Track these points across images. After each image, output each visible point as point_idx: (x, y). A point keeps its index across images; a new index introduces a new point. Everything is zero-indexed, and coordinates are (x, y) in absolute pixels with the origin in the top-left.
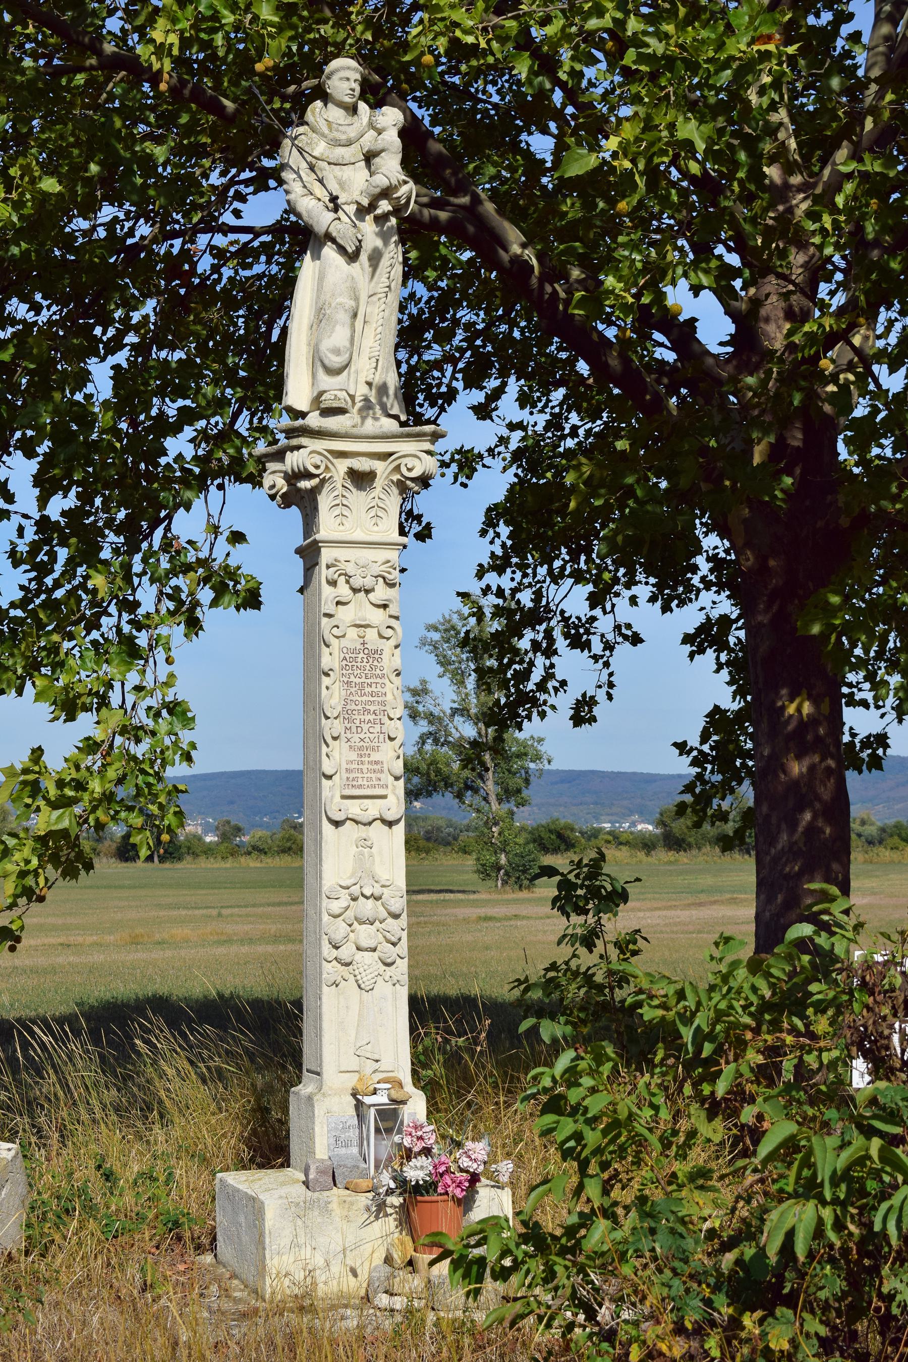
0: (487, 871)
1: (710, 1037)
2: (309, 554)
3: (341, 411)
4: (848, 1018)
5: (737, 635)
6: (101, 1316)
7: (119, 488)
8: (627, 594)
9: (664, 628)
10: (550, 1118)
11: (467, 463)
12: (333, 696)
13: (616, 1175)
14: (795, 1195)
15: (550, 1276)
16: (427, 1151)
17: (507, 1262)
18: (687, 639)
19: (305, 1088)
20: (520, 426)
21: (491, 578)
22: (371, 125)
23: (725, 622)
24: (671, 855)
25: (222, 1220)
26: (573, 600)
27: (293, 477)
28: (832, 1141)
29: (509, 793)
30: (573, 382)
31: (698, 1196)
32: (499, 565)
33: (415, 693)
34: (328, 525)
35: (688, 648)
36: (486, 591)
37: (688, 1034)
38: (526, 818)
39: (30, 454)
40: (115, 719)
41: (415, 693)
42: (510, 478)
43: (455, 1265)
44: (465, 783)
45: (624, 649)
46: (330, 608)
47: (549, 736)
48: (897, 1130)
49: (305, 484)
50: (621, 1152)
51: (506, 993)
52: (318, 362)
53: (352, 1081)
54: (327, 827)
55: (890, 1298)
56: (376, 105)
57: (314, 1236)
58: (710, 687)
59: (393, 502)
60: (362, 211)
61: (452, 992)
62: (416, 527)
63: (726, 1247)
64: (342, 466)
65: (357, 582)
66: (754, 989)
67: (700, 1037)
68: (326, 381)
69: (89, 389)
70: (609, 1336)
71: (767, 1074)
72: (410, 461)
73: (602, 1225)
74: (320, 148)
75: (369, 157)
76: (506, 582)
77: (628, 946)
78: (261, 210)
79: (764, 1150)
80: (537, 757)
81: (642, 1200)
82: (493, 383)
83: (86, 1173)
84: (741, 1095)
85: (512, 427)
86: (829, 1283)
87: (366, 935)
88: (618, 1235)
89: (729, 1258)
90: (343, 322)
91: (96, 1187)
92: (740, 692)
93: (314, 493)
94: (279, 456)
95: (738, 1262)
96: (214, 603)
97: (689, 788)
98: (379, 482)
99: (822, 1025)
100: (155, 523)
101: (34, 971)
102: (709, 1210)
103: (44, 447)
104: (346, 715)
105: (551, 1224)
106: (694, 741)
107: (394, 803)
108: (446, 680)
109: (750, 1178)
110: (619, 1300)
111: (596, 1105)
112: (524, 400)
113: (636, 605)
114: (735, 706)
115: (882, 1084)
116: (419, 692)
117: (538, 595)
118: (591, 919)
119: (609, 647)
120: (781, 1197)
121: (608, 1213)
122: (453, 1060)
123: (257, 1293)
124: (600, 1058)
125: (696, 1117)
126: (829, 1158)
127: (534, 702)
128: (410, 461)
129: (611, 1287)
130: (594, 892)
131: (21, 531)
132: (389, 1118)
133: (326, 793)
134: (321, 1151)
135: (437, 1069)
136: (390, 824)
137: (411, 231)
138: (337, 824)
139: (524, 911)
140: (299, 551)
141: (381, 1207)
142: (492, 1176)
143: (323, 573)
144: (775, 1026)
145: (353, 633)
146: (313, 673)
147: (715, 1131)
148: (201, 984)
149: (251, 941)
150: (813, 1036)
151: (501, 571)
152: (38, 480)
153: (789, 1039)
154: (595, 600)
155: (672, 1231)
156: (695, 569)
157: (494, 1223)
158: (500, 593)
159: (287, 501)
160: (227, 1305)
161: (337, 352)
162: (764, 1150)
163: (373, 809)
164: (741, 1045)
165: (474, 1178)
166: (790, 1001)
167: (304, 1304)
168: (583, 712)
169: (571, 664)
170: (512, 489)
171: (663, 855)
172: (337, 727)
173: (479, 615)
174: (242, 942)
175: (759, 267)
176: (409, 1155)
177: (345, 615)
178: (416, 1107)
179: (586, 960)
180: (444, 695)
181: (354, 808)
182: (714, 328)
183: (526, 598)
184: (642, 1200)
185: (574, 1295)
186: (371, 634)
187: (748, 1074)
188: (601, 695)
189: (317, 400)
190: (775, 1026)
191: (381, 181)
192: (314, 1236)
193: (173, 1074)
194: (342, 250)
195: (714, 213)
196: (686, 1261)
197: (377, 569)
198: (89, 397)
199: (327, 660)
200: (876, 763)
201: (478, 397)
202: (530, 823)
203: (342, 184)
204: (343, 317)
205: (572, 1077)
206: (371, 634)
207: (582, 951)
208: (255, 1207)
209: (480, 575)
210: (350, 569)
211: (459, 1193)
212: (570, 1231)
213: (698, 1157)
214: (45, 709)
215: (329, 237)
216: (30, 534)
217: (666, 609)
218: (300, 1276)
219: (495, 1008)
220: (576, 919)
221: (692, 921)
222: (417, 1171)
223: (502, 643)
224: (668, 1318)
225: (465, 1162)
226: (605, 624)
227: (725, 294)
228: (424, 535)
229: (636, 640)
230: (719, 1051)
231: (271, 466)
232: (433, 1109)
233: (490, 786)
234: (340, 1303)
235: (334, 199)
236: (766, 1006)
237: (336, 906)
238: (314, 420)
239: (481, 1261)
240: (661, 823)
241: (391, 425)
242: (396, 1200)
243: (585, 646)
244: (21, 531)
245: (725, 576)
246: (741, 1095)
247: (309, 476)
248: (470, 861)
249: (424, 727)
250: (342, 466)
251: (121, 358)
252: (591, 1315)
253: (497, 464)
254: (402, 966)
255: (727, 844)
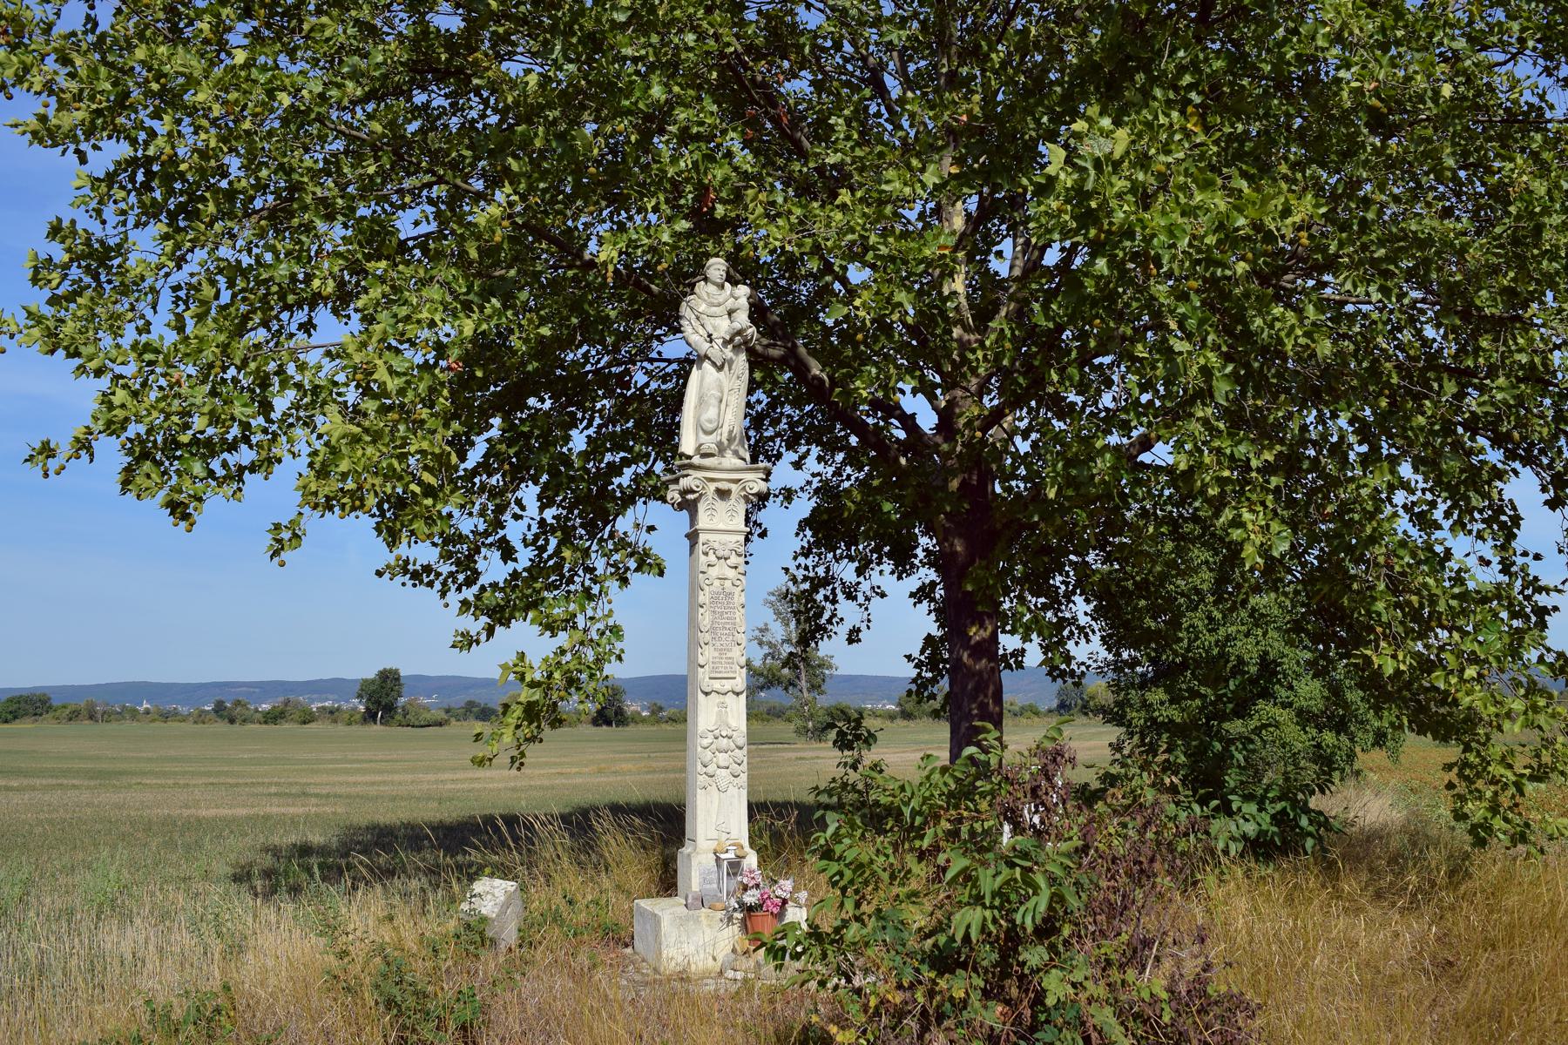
0: (802, 732)
1: (920, 813)
2: (693, 537)
3: (712, 455)
4: (998, 799)
5: (939, 592)
6: (561, 982)
7: (592, 504)
8: (878, 569)
9: (900, 589)
10: (825, 862)
11: (788, 495)
12: (705, 619)
13: (863, 897)
14: (968, 904)
15: (824, 956)
16: (757, 886)
17: (799, 949)
18: (912, 595)
19: (686, 850)
20: (819, 474)
21: (801, 560)
22: (732, 295)
23: (933, 584)
24: (905, 723)
25: (637, 928)
26: (846, 571)
27: (684, 493)
28: (991, 871)
29: (814, 687)
30: (847, 448)
31: (912, 908)
32: (806, 553)
33: (761, 630)
34: (703, 521)
35: (913, 600)
36: (798, 567)
37: (907, 812)
38: (824, 701)
39: (536, 483)
40: (578, 636)
41: (761, 630)
42: (812, 504)
43: (769, 951)
44: (786, 682)
45: (876, 600)
46: (704, 568)
47: (831, 648)
48: (1029, 864)
49: (690, 497)
50: (866, 883)
51: (810, 799)
52: (701, 429)
53: (713, 845)
54: (701, 696)
55: (1024, 963)
56: (735, 283)
57: (692, 938)
58: (924, 622)
59: (741, 508)
60: (726, 343)
61: (780, 800)
62: (755, 530)
63: (927, 936)
64: (712, 487)
65: (720, 553)
66: (946, 784)
67: (914, 813)
68: (704, 438)
69: (571, 445)
70: (858, 991)
71: (953, 835)
72: (751, 484)
73: (855, 926)
74: (702, 307)
75: (730, 313)
76: (810, 562)
77: (876, 767)
78: (672, 348)
79: (949, 875)
80: (830, 667)
81: (879, 910)
82: (803, 449)
83: (558, 900)
84: (936, 849)
85: (813, 475)
86: (988, 956)
87: (722, 759)
88: (864, 932)
89: (930, 942)
90: (715, 403)
91: (563, 906)
92: (941, 626)
93: (696, 501)
94: (676, 481)
95: (935, 945)
96: (636, 570)
97: (914, 681)
98: (733, 496)
99: (984, 805)
100: (606, 523)
101: (542, 788)
102: (918, 918)
103: (545, 478)
104: (712, 630)
105: (826, 928)
106: (916, 654)
107: (740, 682)
108: (779, 623)
109: (942, 896)
110: (866, 971)
111: (850, 855)
112: (820, 459)
113: (883, 575)
114: (939, 634)
115: (1019, 838)
116: (764, 630)
117: (828, 569)
118: (856, 753)
119: (868, 599)
120: (960, 905)
121: (858, 919)
122: (776, 836)
123: (656, 970)
124: (853, 826)
125: (911, 860)
126: (988, 882)
127: (825, 630)
128: (751, 484)
129: (861, 962)
130: (858, 737)
131: (529, 527)
132: (735, 867)
133: (700, 676)
134: (695, 887)
135: (766, 840)
136: (738, 694)
137: (757, 360)
138: (707, 694)
139: (822, 754)
140: (687, 536)
141: (730, 919)
142: (796, 901)
143: (700, 548)
144: (957, 807)
145: (717, 583)
146: (694, 606)
147: (920, 870)
148: (637, 796)
149: (666, 771)
150: (977, 811)
151: (806, 556)
152: (540, 498)
153: (965, 814)
154: (860, 572)
155: (896, 928)
156: (916, 556)
157: (794, 926)
158: (806, 568)
159: (681, 507)
160: (638, 977)
161: (710, 421)
162: (949, 875)
163: (728, 685)
164: (937, 818)
165: (785, 902)
166: (963, 793)
167: (683, 977)
168: (853, 637)
169: (845, 608)
170: (814, 510)
171: (900, 722)
172: (708, 637)
173: (794, 580)
174: (661, 772)
175: (950, 383)
176: (746, 888)
177: (713, 572)
178: (752, 860)
179: (853, 776)
180: (778, 632)
181: (717, 685)
182: (927, 420)
183: (821, 571)
184: (879, 910)
185: (839, 967)
186: (728, 584)
187: (941, 834)
188: (863, 627)
189: (698, 449)
190: (957, 807)
191: (737, 326)
192: (692, 938)
193: (614, 843)
194: (714, 364)
195: (926, 345)
196: (904, 945)
197: (732, 546)
198: (570, 450)
199: (702, 598)
200: (1020, 665)
201: (794, 457)
202: (826, 705)
203: (715, 328)
204: (714, 402)
205: (837, 838)
206: (728, 584)
207: (850, 771)
208: (656, 920)
209: (795, 558)
210: (716, 546)
211: (775, 911)
212: (837, 930)
213: (914, 885)
214: (536, 629)
215: (707, 357)
216: (535, 529)
217: (900, 578)
218: (680, 959)
219: (799, 806)
220: (846, 753)
221: (911, 755)
222: (751, 898)
223: (808, 596)
224: (893, 981)
225: (779, 892)
226: (865, 586)
227: (932, 398)
228: (763, 535)
229: (883, 595)
230: (925, 823)
231: (672, 487)
232: (762, 862)
233: (803, 684)
234: (706, 975)
235: (710, 336)
236: (951, 795)
237: (705, 742)
238: (696, 460)
239: (784, 949)
240: (900, 704)
241: (740, 463)
242: (739, 915)
243: (855, 598)
244: (529, 527)
245: (933, 560)
246: (936, 849)
247: (693, 492)
248: (792, 727)
249: (766, 650)
250: (712, 487)
251: (591, 431)
252: (849, 980)
253: (805, 496)
254: (744, 777)
255: (936, 714)
